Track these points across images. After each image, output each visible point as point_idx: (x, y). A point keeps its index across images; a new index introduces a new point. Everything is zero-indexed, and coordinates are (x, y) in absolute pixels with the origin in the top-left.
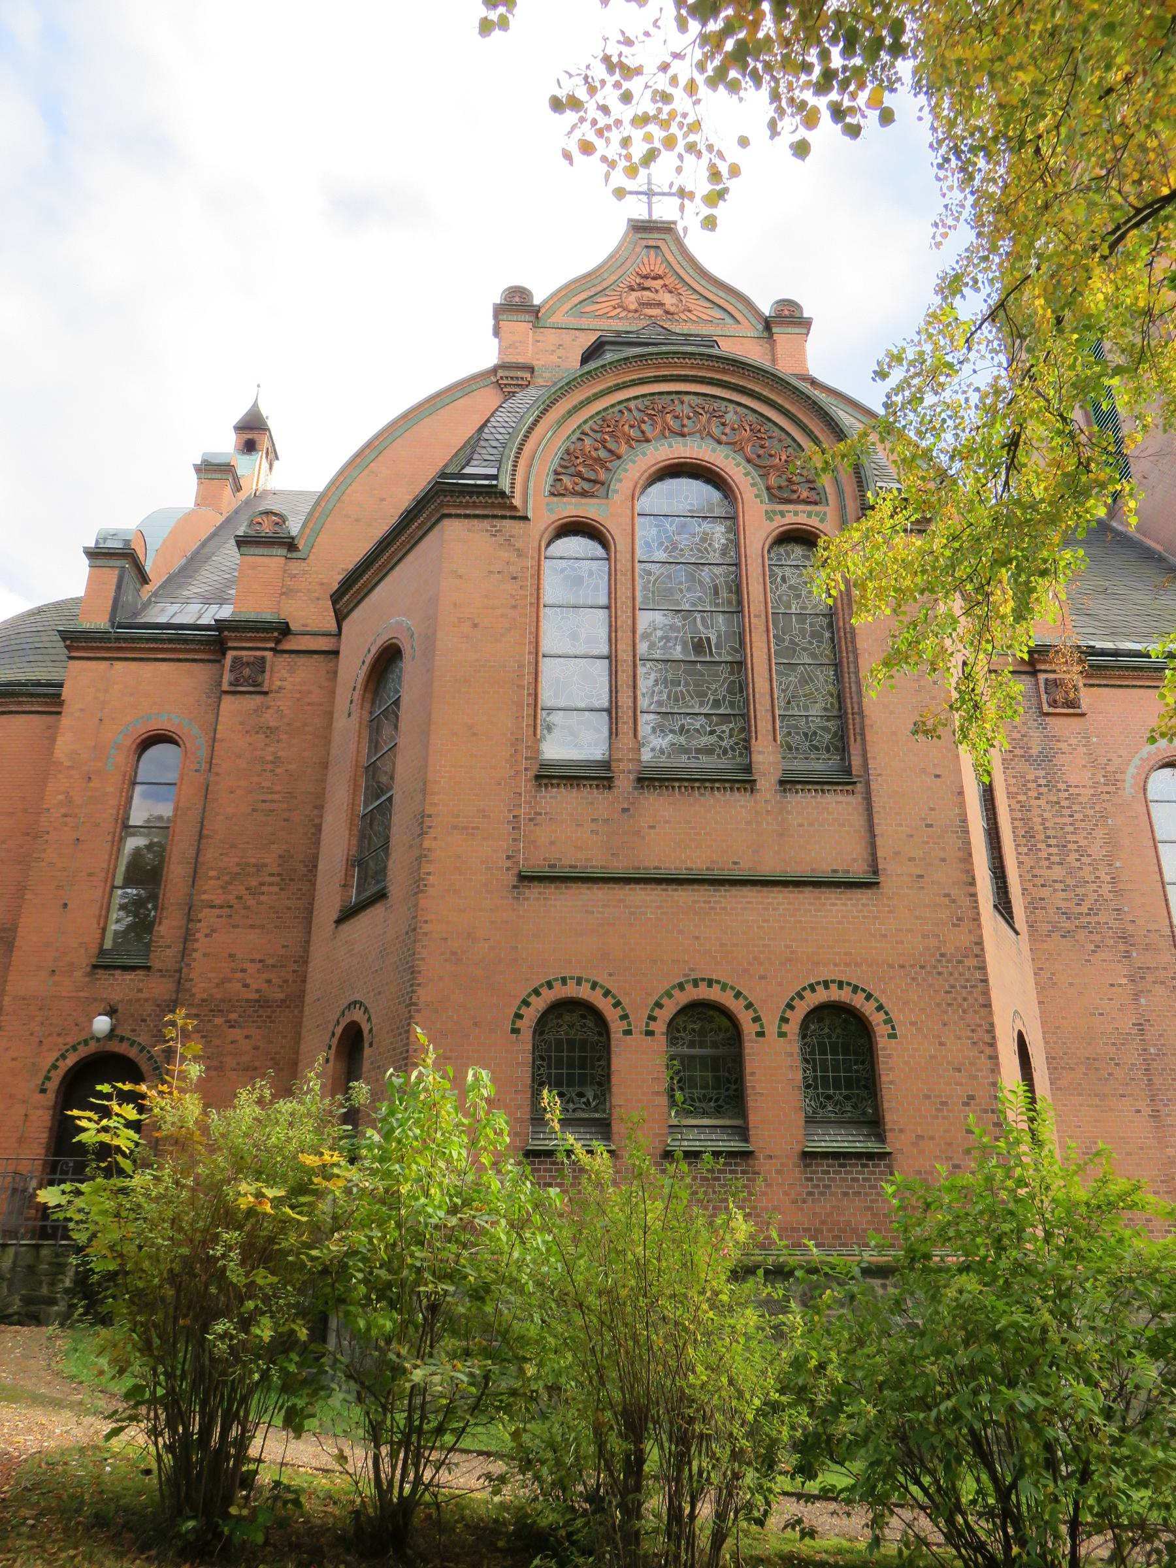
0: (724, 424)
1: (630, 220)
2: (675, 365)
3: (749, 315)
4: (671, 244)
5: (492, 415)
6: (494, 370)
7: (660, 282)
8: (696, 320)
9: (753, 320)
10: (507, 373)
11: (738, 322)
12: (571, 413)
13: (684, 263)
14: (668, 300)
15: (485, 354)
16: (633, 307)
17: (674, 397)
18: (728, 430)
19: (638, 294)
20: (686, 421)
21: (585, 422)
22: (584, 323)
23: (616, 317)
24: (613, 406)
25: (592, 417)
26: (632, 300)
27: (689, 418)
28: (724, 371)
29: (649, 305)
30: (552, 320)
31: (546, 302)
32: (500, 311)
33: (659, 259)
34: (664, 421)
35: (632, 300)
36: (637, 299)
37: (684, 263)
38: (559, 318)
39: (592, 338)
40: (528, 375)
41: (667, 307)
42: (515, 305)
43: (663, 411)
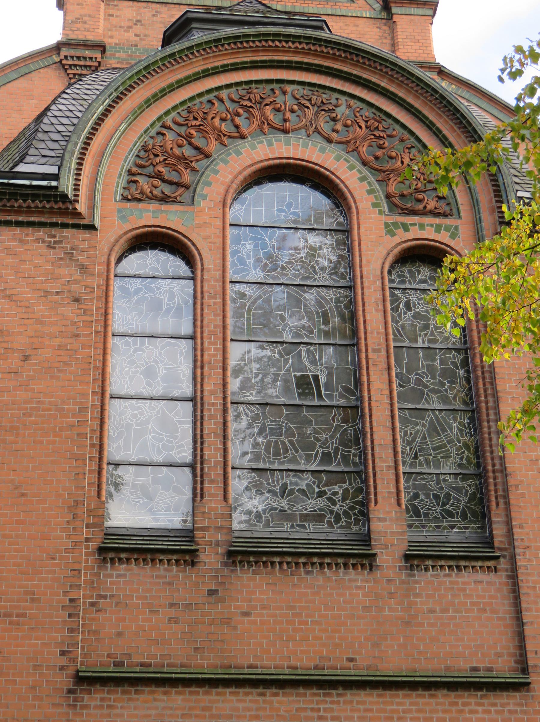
0: (334, 120)
2: (276, 50)
5: (54, 102)
6: (58, 47)
10: (72, 52)
17: (274, 86)
18: (339, 127)
20: (288, 115)
21: (167, 113)
24: (200, 95)
25: (175, 108)
27: (292, 111)
28: (335, 58)
34: (263, 114)
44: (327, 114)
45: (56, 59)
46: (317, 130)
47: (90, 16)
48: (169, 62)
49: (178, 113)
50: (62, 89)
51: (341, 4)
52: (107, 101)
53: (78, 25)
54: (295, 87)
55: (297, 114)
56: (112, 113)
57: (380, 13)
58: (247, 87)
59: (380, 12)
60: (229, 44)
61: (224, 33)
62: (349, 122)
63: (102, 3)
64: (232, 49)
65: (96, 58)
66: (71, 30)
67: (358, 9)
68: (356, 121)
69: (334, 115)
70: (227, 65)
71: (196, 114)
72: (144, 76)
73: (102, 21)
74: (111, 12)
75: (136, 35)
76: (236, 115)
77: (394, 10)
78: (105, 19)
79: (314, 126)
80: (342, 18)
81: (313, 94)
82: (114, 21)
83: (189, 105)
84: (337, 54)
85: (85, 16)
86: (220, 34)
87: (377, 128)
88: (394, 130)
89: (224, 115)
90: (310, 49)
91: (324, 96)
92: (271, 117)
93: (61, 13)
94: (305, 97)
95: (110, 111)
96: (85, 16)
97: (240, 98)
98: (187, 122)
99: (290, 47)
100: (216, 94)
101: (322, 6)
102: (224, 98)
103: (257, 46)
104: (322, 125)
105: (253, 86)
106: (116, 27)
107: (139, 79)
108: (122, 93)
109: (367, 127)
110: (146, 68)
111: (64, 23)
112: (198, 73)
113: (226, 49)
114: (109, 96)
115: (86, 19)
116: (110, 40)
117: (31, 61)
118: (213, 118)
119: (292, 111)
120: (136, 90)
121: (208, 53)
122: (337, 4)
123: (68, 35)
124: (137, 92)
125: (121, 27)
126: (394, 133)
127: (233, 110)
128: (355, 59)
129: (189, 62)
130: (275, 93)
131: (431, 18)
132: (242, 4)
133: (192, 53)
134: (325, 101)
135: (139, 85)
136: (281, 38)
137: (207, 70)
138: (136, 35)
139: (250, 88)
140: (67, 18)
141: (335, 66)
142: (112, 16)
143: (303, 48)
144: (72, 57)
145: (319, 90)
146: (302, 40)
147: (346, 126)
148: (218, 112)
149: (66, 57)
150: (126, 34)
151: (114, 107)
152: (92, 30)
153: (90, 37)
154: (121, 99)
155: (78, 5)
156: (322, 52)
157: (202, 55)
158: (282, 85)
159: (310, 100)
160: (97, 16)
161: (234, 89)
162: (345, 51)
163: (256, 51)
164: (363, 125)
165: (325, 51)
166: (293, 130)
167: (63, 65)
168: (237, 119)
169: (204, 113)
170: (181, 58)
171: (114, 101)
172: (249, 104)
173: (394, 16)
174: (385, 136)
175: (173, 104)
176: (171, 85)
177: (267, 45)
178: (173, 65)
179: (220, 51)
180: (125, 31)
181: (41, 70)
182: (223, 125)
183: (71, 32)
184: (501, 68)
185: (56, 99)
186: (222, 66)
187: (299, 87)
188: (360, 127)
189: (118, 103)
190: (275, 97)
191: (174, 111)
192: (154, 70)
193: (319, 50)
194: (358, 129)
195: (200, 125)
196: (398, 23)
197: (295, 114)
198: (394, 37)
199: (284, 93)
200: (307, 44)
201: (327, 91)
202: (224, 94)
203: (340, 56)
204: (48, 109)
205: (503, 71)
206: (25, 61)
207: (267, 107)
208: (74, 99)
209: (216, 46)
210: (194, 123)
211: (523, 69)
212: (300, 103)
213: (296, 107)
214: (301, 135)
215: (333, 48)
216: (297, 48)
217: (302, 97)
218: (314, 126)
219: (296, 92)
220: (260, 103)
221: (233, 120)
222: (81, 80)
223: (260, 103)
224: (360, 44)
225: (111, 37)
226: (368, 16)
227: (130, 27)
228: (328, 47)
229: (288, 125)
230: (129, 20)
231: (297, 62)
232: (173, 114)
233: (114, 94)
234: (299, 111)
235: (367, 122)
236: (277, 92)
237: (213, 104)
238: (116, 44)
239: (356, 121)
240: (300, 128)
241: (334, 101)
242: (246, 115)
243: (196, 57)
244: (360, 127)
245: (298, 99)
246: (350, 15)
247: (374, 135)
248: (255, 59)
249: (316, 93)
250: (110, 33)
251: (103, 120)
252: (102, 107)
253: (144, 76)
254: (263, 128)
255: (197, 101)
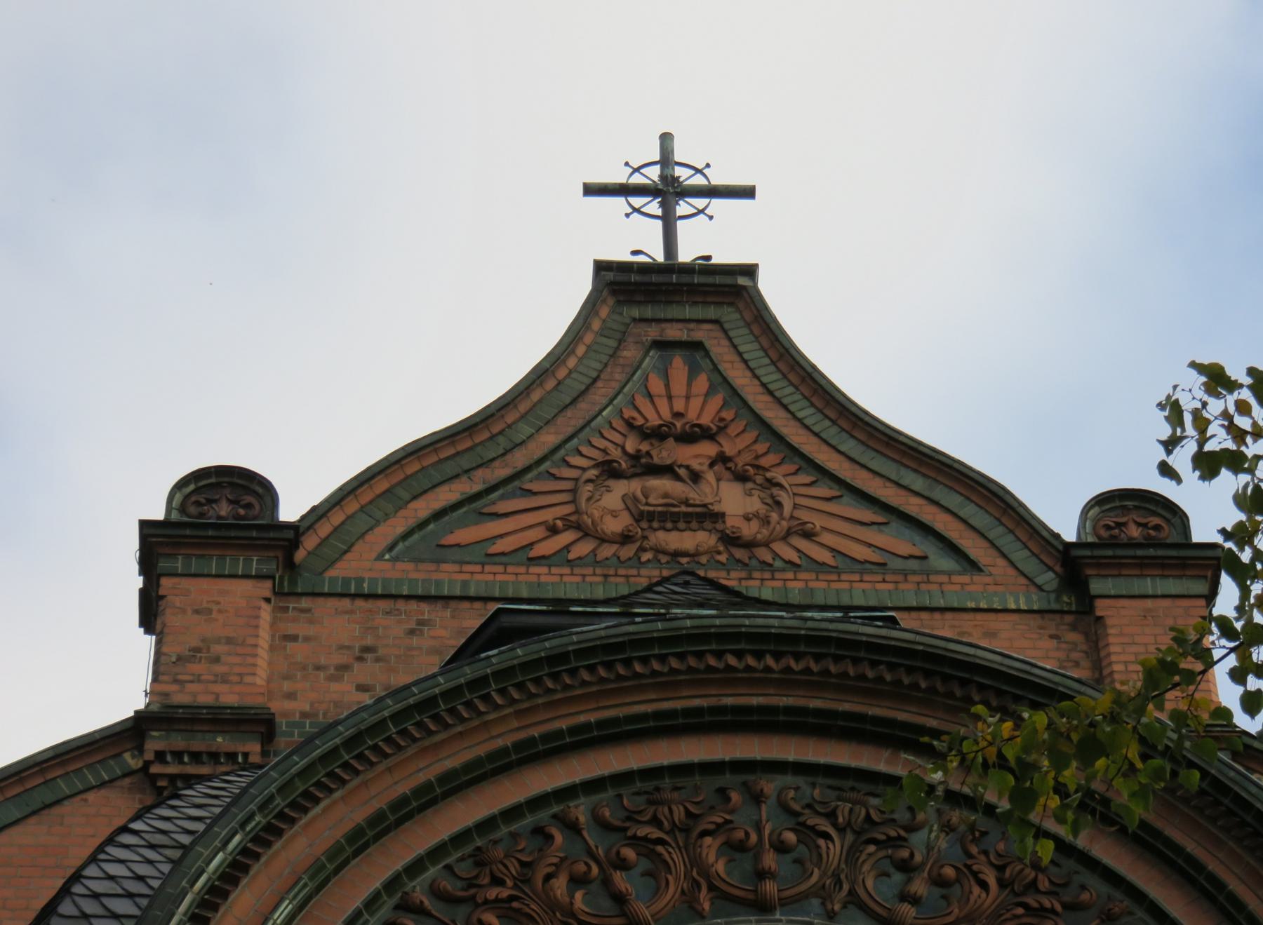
0: (906, 867)
1: (601, 267)
2: (729, 678)
3: (1007, 542)
4: (741, 335)
5: (93, 859)
6: (134, 730)
7: (708, 449)
8: (834, 566)
9: (1020, 555)
10: (178, 742)
11: (974, 566)
12: (360, 841)
13: (786, 392)
14: (734, 501)
15: (97, 673)
16: (614, 526)
17: (727, 779)
18: (919, 887)
19: (635, 486)
20: (770, 860)
21: (415, 868)
22: (449, 577)
23: (560, 558)
24: (512, 814)
25: (436, 853)
26: (611, 505)
27: (781, 848)
28: (899, 694)
29: (671, 517)
30: (343, 570)
31: (317, 514)
32: (158, 545)
33: (702, 383)
34: (696, 862)
35: (611, 505)
36: (630, 502)
37: (786, 392)
38: (362, 563)
39: (472, 619)
40: (254, 748)
41: (733, 522)
42: (212, 531)
43: (688, 829)
44: (882, 853)
45: (132, 761)
46: (854, 900)
47: (229, 641)
48: (419, 725)
49: (448, 867)
50: (119, 822)
51: (944, 579)
52: (237, 838)
53: (196, 668)
54: (789, 779)
55: (794, 855)
56: (252, 873)
57: (1058, 599)
58: (649, 785)
59: (1058, 592)
60: (591, 669)
61: (575, 638)
62: (949, 872)
63: (264, 605)
64: (602, 680)
65: (246, 755)
66: (176, 681)
67: (991, 588)
68: (966, 866)
69: (905, 854)
70: (587, 727)
71: (498, 869)
72: (346, 766)
73: (263, 653)
74: (291, 629)
75: (362, 688)
76: (616, 867)
77: (1096, 587)
78: (272, 648)
79: (846, 887)
80: (949, 615)
81: (839, 799)
82: (299, 651)
83: (479, 843)
84: (906, 681)
85: (218, 641)
86: (565, 640)
87: (1033, 885)
88: (1083, 887)
89: (581, 868)
90: (826, 672)
91: (874, 801)
92: (720, 867)
93: (148, 642)
94: (818, 808)
95: (245, 869)
96: (218, 641)
97: (629, 818)
98: (472, 891)
99: (768, 669)
100: (556, 809)
101: (891, 586)
102: (582, 819)
103: (673, 671)
104: (870, 883)
105: (667, 782)
106: (304, 668)
107: (331, 775)
108: (281, 816)
109: (1002, 884)
110: (351, 743)
111: (156, 662)
112: (504, 752)
113: (584, 683)
114: (243, 825)
115: (218, 649)
116: (288, 705)
117: (60, 772)
118: (548, 877)
119: (781, 848)
120: (322, 805)
121: (532, 696)
122: (932, 578)
123: (166, 695)
124: (324, 810)
125: (318, 668)
126: (1085, 896)
127: (607, 852)
128: (958, 693)
129: (476, 723)
130: (729, 799)
131: (1202, 602)
132: (660, 589)
133: (486, 698)
134: (875, 816)
135: (331, 791)
136: (742, 646)
137: (531, 742)
138: (362, 688)
139: (657, 789)
140: (165, 649)
141: (902, 716)
142: (294, 638)
143: (807, 671)
144: (178, 755)
145: (857, 785)
146: (802, 648)
147: (939, 882)
148: (562, 860)
149: (160, 756)
150: (334, 686)
151: (257, 856)
152: (235, 679)
153: (230, 698)
154: (279, 833)
155: (197, 612)
156: (862, 677)
157: (514, 701)
158: (750, 778)
159: (831, 816)
160: (251, 641)
161: (611, 793)
162: (928, 674)
163: (669, 684)
164: (991, 879)
165: (870, 674)
166: (785, 903)
167: (153, 778)
168: (619, 878)
169: (523, 864)
170: (452, 711)
171: (256, 839)
172: (656, 834)
173: (1099, 603)
174: (1058, 908)
175: (433, 842)
176: (426, 788)
177: (702, 667)
178: (430, 733)
179: (567, 687)
180: (331, 678)
181: (91, 796)
182: (579, 895)
183: (174, 687)
184: (1164, 437)
185: (101, 849)
186: (573, 730)
187: (800, 781)
188: (984, 885)
189: (268, 844)
190: (732, 812)
191: (434, 864)
192: (375, 748)
193: (851, 672)
194: (976, 890)
195: (512, 898)
196: (1109, 622)
197: (788, 858)
198: (1099, 660)
199: (757, 798)
200: (818, 657)
201: (880, 789)
202: (580, 810)
203: (915, 686)
204: (76, 877)
205: (1170, 444)
206: (42, 772)
207: (708, 840)
208: (152, 846)
209: (555, 676)
210: (493, 893)
211: (1243, 448)
212: (803, 824)
213: (790, 837)
214: (808, 914)
215: (892, 667)
216: (788, 670)
217: (809, 806)
218: (846, 887)
219: (792, 794)
220: (686, 830)
221: (606, 882)
222: (178, 797)
223: (686, 830)
224: (972, 651)
225: (291, 696)
226: (1023, 607)
227: (344, 668)
228: (879, 663)
229: (770, 887)
230: (342, 647)
231: (789, 710)
232: (432, 871)
233: (257, 818)
234: (802, 848)
235: (1000, 869)
236: (735, 797)
237: (550, 838)
238: (304, 715)
239: (969, 867)
240: (805, 896)
241: (902, 816)
242: (644, 864)
243: (497, 707)
244: (984, 885)
245: (796, 814)
246: (971, 605)
247: (1025, 906)
248: (666, 705)
249: (854, 795)
250: (287, 686)
251: (225, 895)
252: (220, 856)
253: (346, 766)
254: (698, 901)
255: (504, 830)
